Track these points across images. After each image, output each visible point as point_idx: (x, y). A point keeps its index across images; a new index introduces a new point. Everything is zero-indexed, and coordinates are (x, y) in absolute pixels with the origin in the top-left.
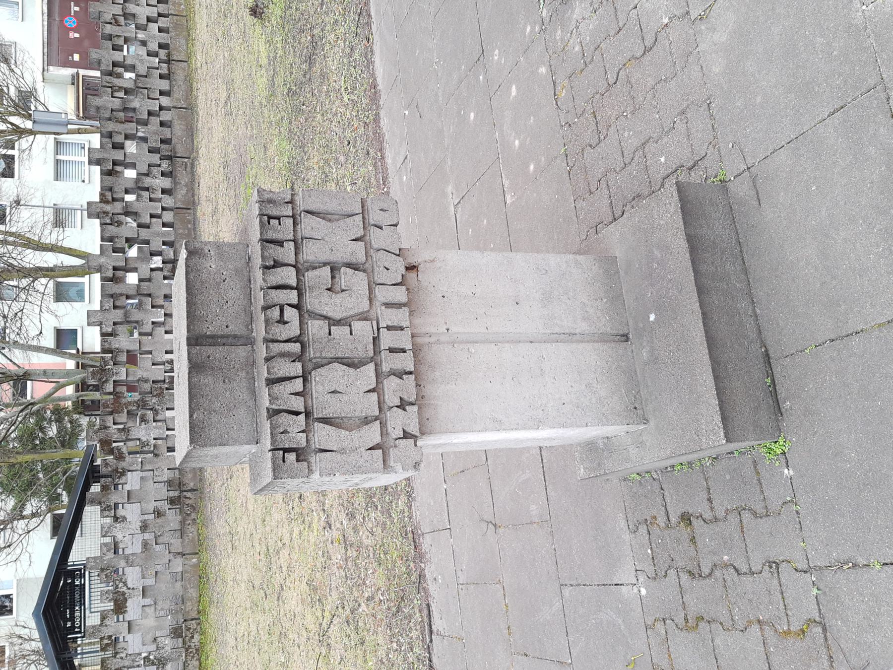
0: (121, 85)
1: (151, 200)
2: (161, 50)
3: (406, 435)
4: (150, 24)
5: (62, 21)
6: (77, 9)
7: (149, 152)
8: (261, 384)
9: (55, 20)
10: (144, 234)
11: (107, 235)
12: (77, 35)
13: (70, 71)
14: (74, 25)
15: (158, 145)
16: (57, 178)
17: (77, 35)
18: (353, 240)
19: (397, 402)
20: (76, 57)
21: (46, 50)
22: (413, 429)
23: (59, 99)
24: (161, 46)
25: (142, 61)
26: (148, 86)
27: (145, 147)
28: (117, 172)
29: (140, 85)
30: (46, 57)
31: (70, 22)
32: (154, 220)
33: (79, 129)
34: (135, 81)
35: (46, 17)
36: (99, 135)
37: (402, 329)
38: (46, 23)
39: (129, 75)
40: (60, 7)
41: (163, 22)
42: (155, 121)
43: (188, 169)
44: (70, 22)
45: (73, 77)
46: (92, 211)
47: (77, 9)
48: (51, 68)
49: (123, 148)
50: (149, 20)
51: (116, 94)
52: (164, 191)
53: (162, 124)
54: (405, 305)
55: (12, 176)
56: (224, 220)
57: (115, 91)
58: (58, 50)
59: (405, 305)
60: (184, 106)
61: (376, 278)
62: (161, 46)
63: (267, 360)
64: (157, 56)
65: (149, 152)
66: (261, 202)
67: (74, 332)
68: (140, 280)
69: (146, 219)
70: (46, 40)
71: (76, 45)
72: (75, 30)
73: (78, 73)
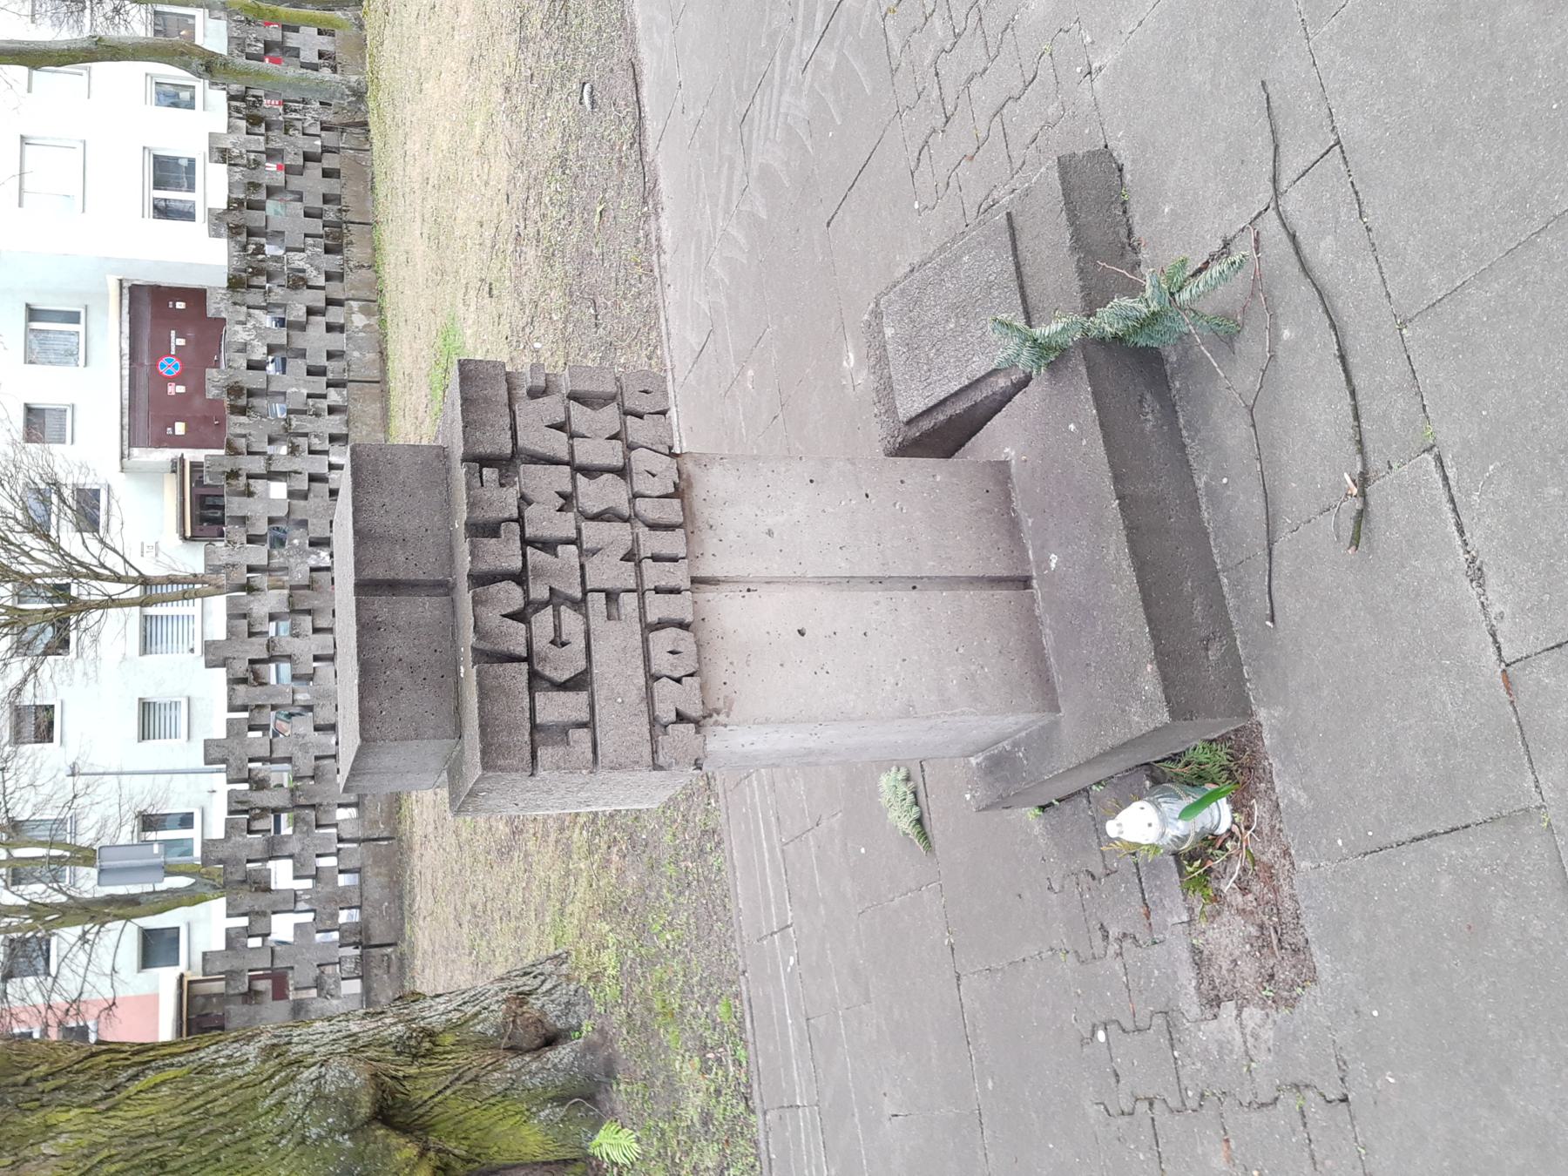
0: (265, 804)
1: (316, 630)
2: (326, 207)
3: (681, 718)
4: (309, 164)
5: (154, 366)
6: (181, 342)
9: (142, 365)
11: (238, 702)
12: (181, 389)
13: (167, 455)
15: (319, 204)
17: (181, 389)
19: (673, 717)
20: (180, 428)
21: (126, 420)
22: (694, 710)
23: (146, 524)
24: (326, 199)
25: (304, 747)
26: (316, 801)
27: (298, 208)
29: (302, 801)
30: (126, 433)
31: (169, 367)
32: (315, 485)
33: (185, 592)
34: (292, 791)
35: (126, 362)
37: (674, 560)
38: (126, 372)
40: (152, 342)
41: (335, 316)
42: (314, 170)
43: (393, 970)
44: (169, 367)
45: (174, 463)
47: (181, 342)
48: (135, 451)
49: (264, 209)
51: (257, 825)
52: (333, 439)
54: (680, 526)
55: (51, 741)
57: (254, 818)
58: (148, 418)
59: (680, 526)
60: (385, 834)
62: (326, 199)
64: (320, 216)
68: (292, 494)
69: (309, 666)
70: (126, 402)
71: (179, 407)
72: (177, 380)
73: (182, 459)
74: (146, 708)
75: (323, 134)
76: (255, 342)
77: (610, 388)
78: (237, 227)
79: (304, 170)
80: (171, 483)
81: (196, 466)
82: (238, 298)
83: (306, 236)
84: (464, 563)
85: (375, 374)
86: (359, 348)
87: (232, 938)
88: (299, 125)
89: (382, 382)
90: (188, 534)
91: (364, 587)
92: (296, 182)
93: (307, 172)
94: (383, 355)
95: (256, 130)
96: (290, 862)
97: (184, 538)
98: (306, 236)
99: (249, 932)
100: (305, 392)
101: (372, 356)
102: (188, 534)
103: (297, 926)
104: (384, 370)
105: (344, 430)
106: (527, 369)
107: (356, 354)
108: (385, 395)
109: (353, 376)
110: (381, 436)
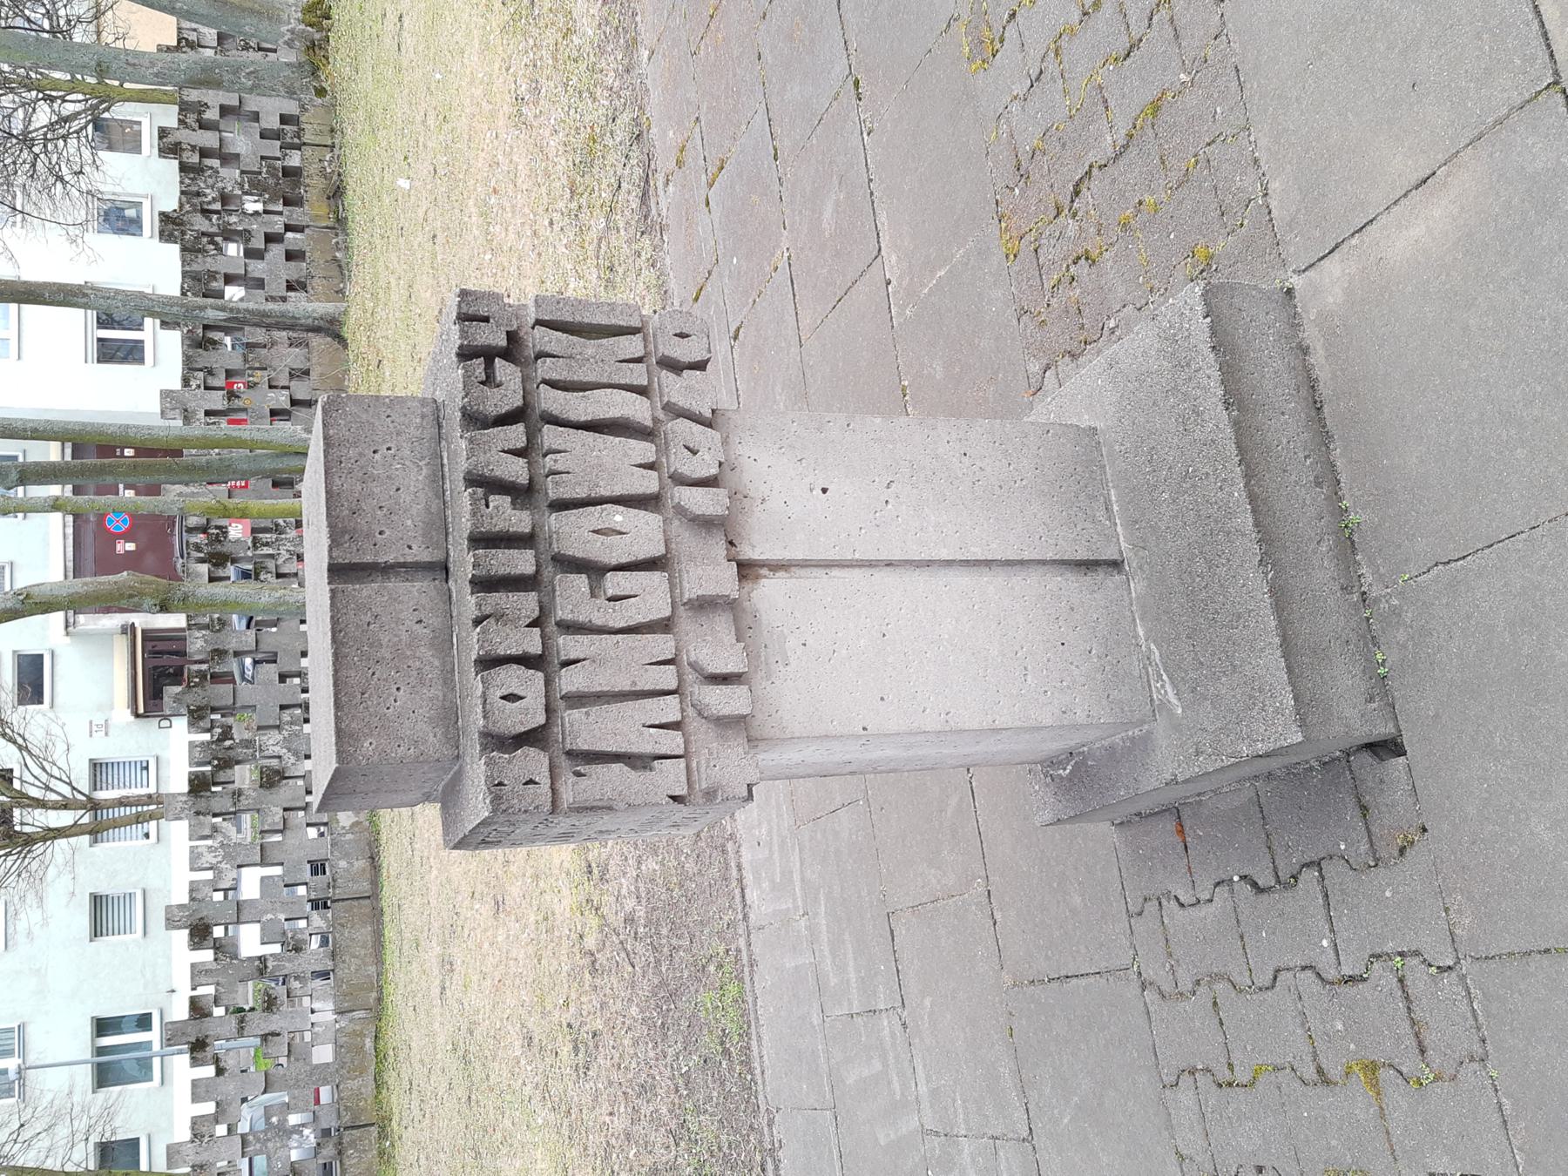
7: (262, 137)
8: (472, 745)
10: (257, 268)
12: (131, 547)
14: (123, 527)
16: (97, 931)
17: (131, 547)
18: (640, 466)
24: (284, 119)
28: (214, 342)
36: (176, 108)
38: (70, 531)
39: (233, 249)
42: (277, 251)
46: (170, 226)
50: (270, 238)
53: (290, 256)
56: (403, 350)
61: (661, 347)
62: (284, 119)
63: (477, 622)
65: (262, 137)
66: (464, 318)
67: (134, 1144)
69: (258, 243)
70: (70, 564)
72: (127, 536)
74: (98, 902)
75: (286, 210)
76: (223, 865)
77: (637, 324)
78: (200, 708)
79: (266, 199)
80: (121, 647)
81: (149, 636)
82: (202, 804)
83: (282, 707)
84: (463, 524)
85: (364, 887)
86: (346, 856)
87: (199, 1128)
88: (271, 564)
89: (374, 896)
90: (141, 710)
91: (338, 572)
92: (257, 268)
93: (268, 256)
94: (374, 860)
95: (220, 573)
96: (257, 927)
97: (137, 716)
98: (282, 707)
99: (216, 1119)
100: (282, 917)
101: (361, 863)
102: (141, 710)
103: (263, 879)
104: (375, 882)
105: (329, 965)
106: (531, 303)
107: (343, 864)
108: (377, 915)
109: (339, 893)
110: (372, 969)
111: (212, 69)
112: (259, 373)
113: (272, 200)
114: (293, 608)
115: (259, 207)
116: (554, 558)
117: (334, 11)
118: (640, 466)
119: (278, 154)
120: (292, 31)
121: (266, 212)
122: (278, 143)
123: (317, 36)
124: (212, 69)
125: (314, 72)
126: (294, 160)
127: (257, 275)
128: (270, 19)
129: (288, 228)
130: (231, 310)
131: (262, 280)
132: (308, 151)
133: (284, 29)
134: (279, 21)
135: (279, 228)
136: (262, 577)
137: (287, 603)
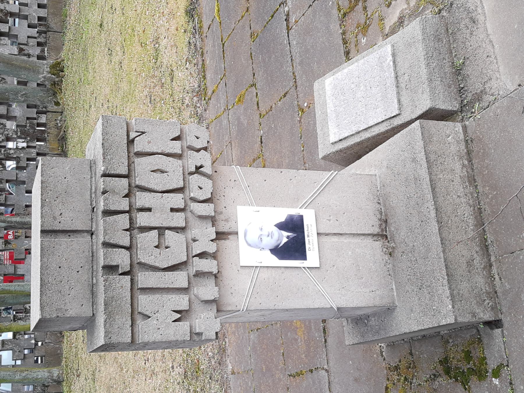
18: (174, 311)
24: (40, 19)
69: (23, 163)
111: (5, 93)
112: (21, 231)
113: (31, 140)
114: (31, 381)
115: (25, 145)
116: (138, 263)
117: (65, 69)
118: (174, 311)
119: (35, 116)
120: (44, 77)
121: (28, 147)
122: (35, 110)
123: (57, 80)
124: (5, 93)
125: (55, 94)
126: (43, 119)
127: (22, 179)
128: (34, 71)
129: (38, 154)
130: (8, 222)
131: (25, 181)
132: (50, 115)
133: (40, 76)
134: (39, 73)
135: (34, 155)
136: (17, 337)
137: (28, 378)
